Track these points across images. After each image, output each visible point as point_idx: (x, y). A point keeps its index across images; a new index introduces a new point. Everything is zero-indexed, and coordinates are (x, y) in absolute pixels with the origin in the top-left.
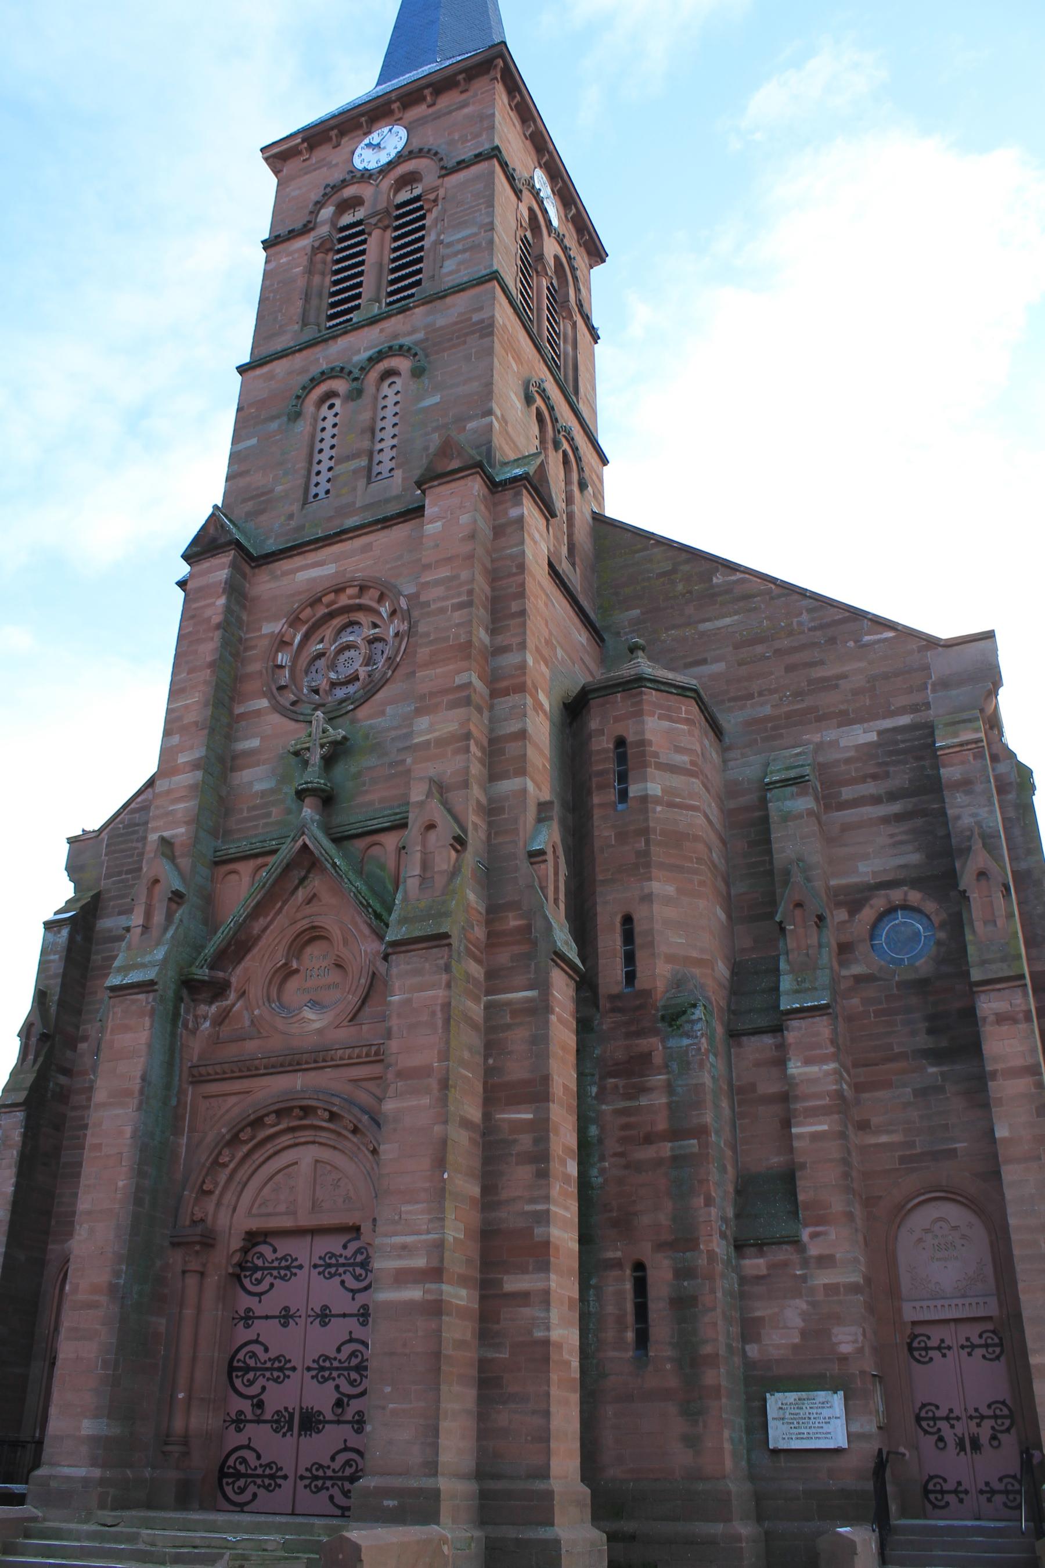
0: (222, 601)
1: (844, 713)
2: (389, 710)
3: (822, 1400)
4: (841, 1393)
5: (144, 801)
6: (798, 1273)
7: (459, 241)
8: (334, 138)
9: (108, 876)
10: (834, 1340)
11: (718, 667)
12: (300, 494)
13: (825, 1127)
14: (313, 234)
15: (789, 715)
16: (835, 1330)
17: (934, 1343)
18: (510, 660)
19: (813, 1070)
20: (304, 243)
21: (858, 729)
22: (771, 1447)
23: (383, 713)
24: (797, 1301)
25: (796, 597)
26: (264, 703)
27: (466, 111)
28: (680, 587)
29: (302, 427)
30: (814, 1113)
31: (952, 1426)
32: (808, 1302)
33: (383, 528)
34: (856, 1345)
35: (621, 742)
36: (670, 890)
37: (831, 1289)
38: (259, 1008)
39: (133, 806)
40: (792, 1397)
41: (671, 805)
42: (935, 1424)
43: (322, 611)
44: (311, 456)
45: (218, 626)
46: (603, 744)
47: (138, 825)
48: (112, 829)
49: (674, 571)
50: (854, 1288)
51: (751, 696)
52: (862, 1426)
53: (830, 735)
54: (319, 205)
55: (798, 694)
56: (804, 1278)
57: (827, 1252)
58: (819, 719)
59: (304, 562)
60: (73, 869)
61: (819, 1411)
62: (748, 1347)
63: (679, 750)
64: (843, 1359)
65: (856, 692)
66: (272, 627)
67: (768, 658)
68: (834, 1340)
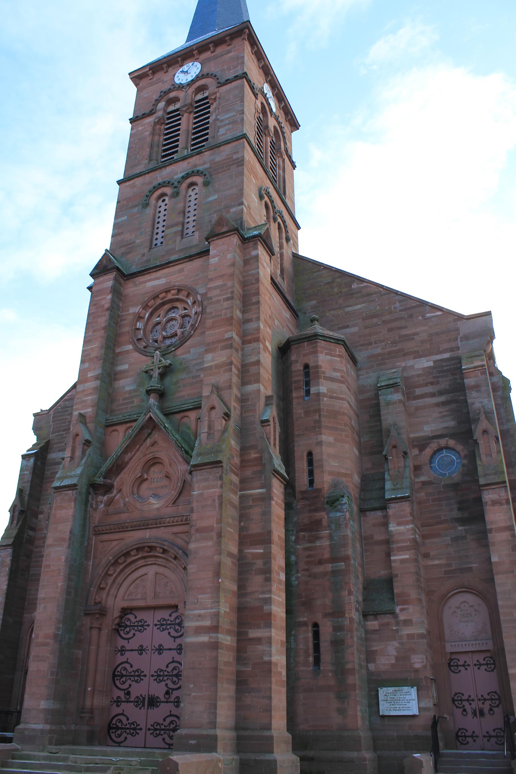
0: (110, 297)
1: (417, 352)
2: (192, 350)
3: (406, 691)
4: (415, 688)
5: (71, 395)
6: (394, 628)
7: (226, 119)
8: (165, 68)
9: (53, 432)
10: (412, 661)
11: (355, 329)
12: (148, 244)
13: (407, 557)
14: (154, 116)
15: (389, 353)
16: (413, 657)
17: (461, 663)
18: (252, 325)
19: (402, 528)
20: (150, 120)
21: (423, 360)
22: (381, 714)
23: (189, 352)
24: (394, 642)
25: (393, 295)
26: (130, 347)
27: (230, 55)
28: (336, 290)
29: (149, 211)
30: (402, 549)
31: (470, 704)
32: (399, 643)
33: (189, 261)
34: (423, 664)
35: (306, 366)
36: (331, 439)
37: (410, 636)
38: (128, 497)
39: (65, 398)
40: (391, 689)
41: (331, 397)
42: (462, 703)
43: (159, 301)
44: (154, 220)
45: (108, 309)
46: (298, 367)
47: (68, 407)
48: (55, 409)
49: (333, 282)
50: (422, 636)
51: (371, 344)
52: (426, 704)
53: (410, 363)
54: (158, 101)
55: (394, 343)
56: (397, 631)
57: (408, 618)
58: (404, 355)
59: (150, 278)
60: (36, 429)
61: (404, 696)
62: (369, 665)
63: (335, 370)
64: (417, 671)
65: (423, 342)
66: (134, 310)
67: (379, 325)
68: (412, 661)
